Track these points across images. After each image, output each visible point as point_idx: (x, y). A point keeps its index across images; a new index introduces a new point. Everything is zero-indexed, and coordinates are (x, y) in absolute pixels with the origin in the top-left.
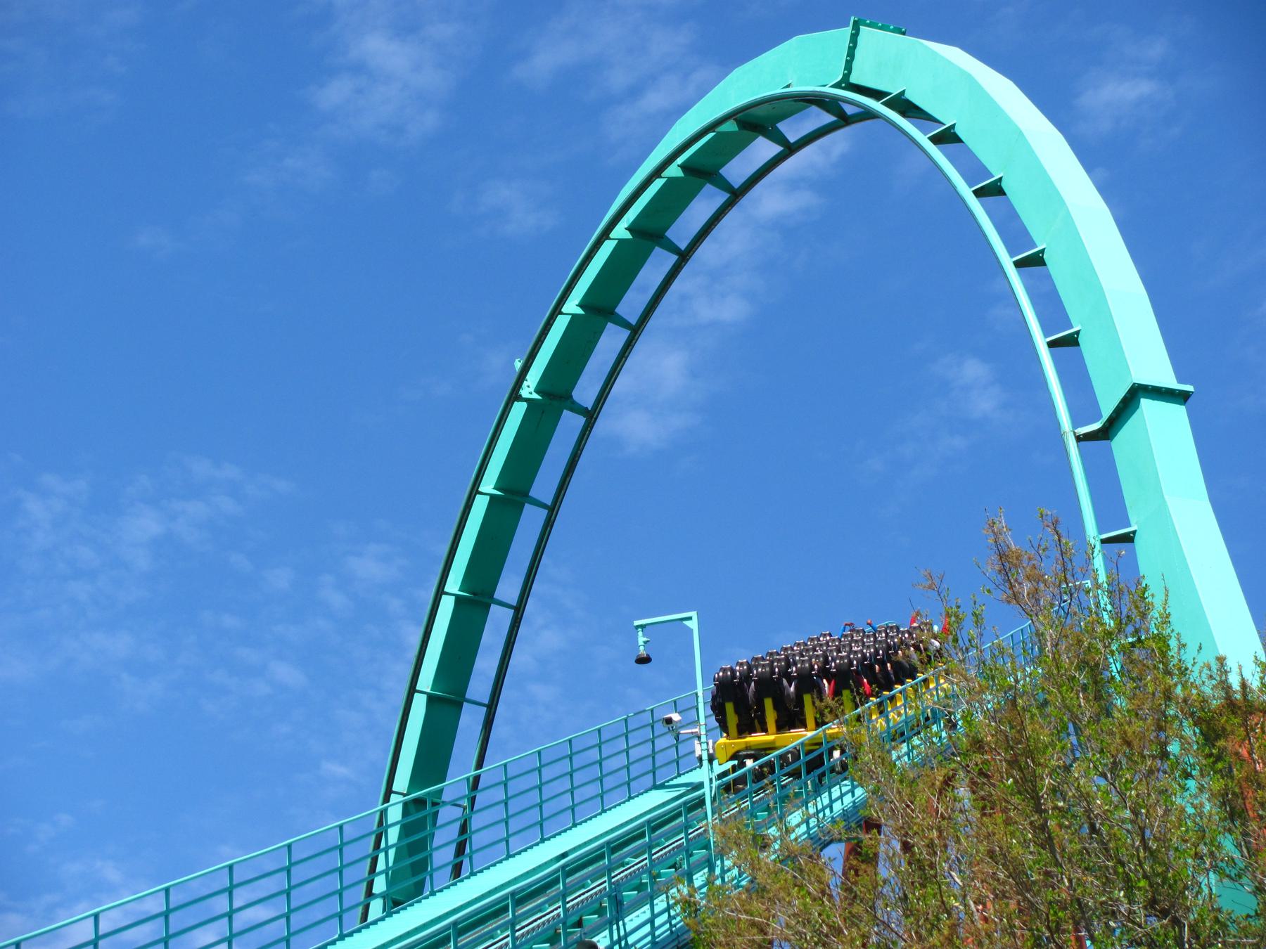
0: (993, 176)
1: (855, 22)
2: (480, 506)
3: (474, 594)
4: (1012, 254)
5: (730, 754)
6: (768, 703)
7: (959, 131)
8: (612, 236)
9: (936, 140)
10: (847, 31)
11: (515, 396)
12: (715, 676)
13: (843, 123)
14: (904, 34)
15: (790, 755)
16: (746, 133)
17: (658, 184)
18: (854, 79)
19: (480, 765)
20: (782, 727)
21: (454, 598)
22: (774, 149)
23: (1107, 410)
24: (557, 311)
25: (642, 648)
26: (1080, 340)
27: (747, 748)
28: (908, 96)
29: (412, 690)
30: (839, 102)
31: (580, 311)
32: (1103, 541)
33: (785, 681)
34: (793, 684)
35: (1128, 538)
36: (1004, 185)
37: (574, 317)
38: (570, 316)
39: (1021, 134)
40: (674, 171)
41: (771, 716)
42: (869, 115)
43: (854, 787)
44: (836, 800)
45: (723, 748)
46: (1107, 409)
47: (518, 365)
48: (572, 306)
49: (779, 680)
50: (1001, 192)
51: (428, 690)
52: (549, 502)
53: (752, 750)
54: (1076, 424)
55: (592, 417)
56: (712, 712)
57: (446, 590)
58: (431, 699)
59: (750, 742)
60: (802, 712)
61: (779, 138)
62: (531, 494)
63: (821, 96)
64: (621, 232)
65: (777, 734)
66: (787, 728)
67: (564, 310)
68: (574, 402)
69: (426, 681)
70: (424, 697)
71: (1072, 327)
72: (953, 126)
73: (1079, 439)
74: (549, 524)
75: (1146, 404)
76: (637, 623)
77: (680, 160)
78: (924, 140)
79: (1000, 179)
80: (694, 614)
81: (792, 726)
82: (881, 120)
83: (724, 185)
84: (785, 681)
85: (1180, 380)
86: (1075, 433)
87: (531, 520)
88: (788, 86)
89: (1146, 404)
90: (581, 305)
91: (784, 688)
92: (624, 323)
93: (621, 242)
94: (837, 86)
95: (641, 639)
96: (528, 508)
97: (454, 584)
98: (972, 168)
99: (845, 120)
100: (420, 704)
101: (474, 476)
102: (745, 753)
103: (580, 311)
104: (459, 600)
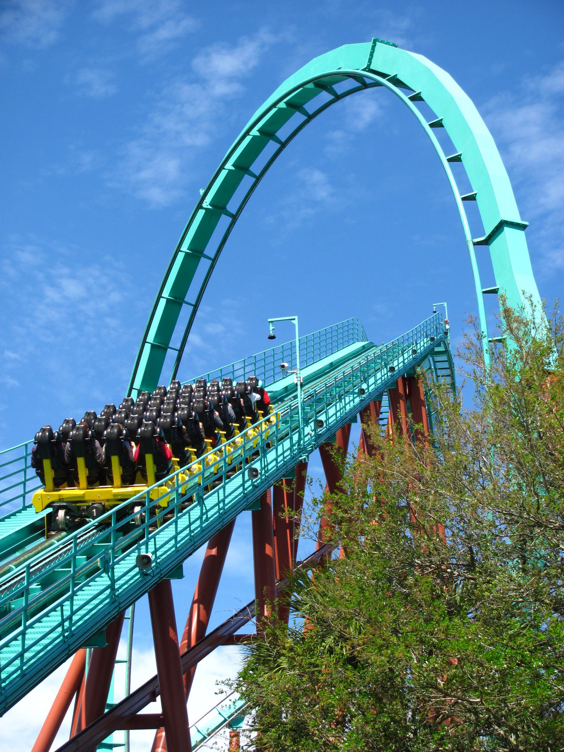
0: (438, 118)
1: (374, 40)
2: (180, 257)
3: (176, 298)
5: (47, 502)
6: (81, 462)
7: (423, 95)
8: (250, 134)
9: (412, 99)
10: (370, 44)
11: (200, 207)
12: (36, 435)
13: (364, 87)
14: (396, 47)
15: (94, 510)
16: (318, 89)
17: (274, 110)
18: (372, 67)
20: (91, 483)
21: (166, 299)
22: (331, 97)
23: (488, 232)
24: (222, 168)
25: (271, 332)
26: (477, 198)
27: (60, 500)
28: (398, 77)
29: (145, 342)
30: (364, 78)
31: (233, 168)
32: (484, 292)
33: (97, 443)
34: (104, 446)
35: (495, 291)
37: (230, 171)
38: (228, 171)
39: (453, 99)
40: (282, 105)
41: (83, 473)
42: (378, 84)
43: (354, 398)
44: (351, 401)
45: (39, 499)
46: (488, 230)
47: (202, 192)
48: (229, 166)
49: (92, 442)
51: (152, 342)
52: (213, 257)
53: (65, 502)
54: (473, 237)
55: (235, 218)
57: (162, 296)
58: (153, 346)
59: (62, 495)
60: (110, 471)
61: (333, 92)
62: (204, 253)
63: (354, 74)
64: (255, 132)
65: (88, 489)
66: (98, 482)
67: (225, 167)
68: (227, 211)
70: (150, 345)
71: (473, 192)
72: (420, 93)
73: (475, 244)
74: (212, 267)
75: (507, 229)
76: (269, 320)
77: (285, 100)
78: (406, 99)
79: (442, 120)
81: (103, 483)
82: (384, 87)
83: (305, 113)
84: (97, 443)
86: (473, 241)
87: (204, 265)
88: (340, 68)
89: (507, 229)
90: (233, 165)
91: (96, 449)
92: (253, 175)
93: (255, 137)
94: (364, 70)
95: (271, 328)
96: (203, 259)
97: (166, 293)
98: (428, 112)
99: (365, 86)
100: (147, 348)
101: (178, 243)
102: (58, 504)
103: (233, 168)
104: (168, 301)
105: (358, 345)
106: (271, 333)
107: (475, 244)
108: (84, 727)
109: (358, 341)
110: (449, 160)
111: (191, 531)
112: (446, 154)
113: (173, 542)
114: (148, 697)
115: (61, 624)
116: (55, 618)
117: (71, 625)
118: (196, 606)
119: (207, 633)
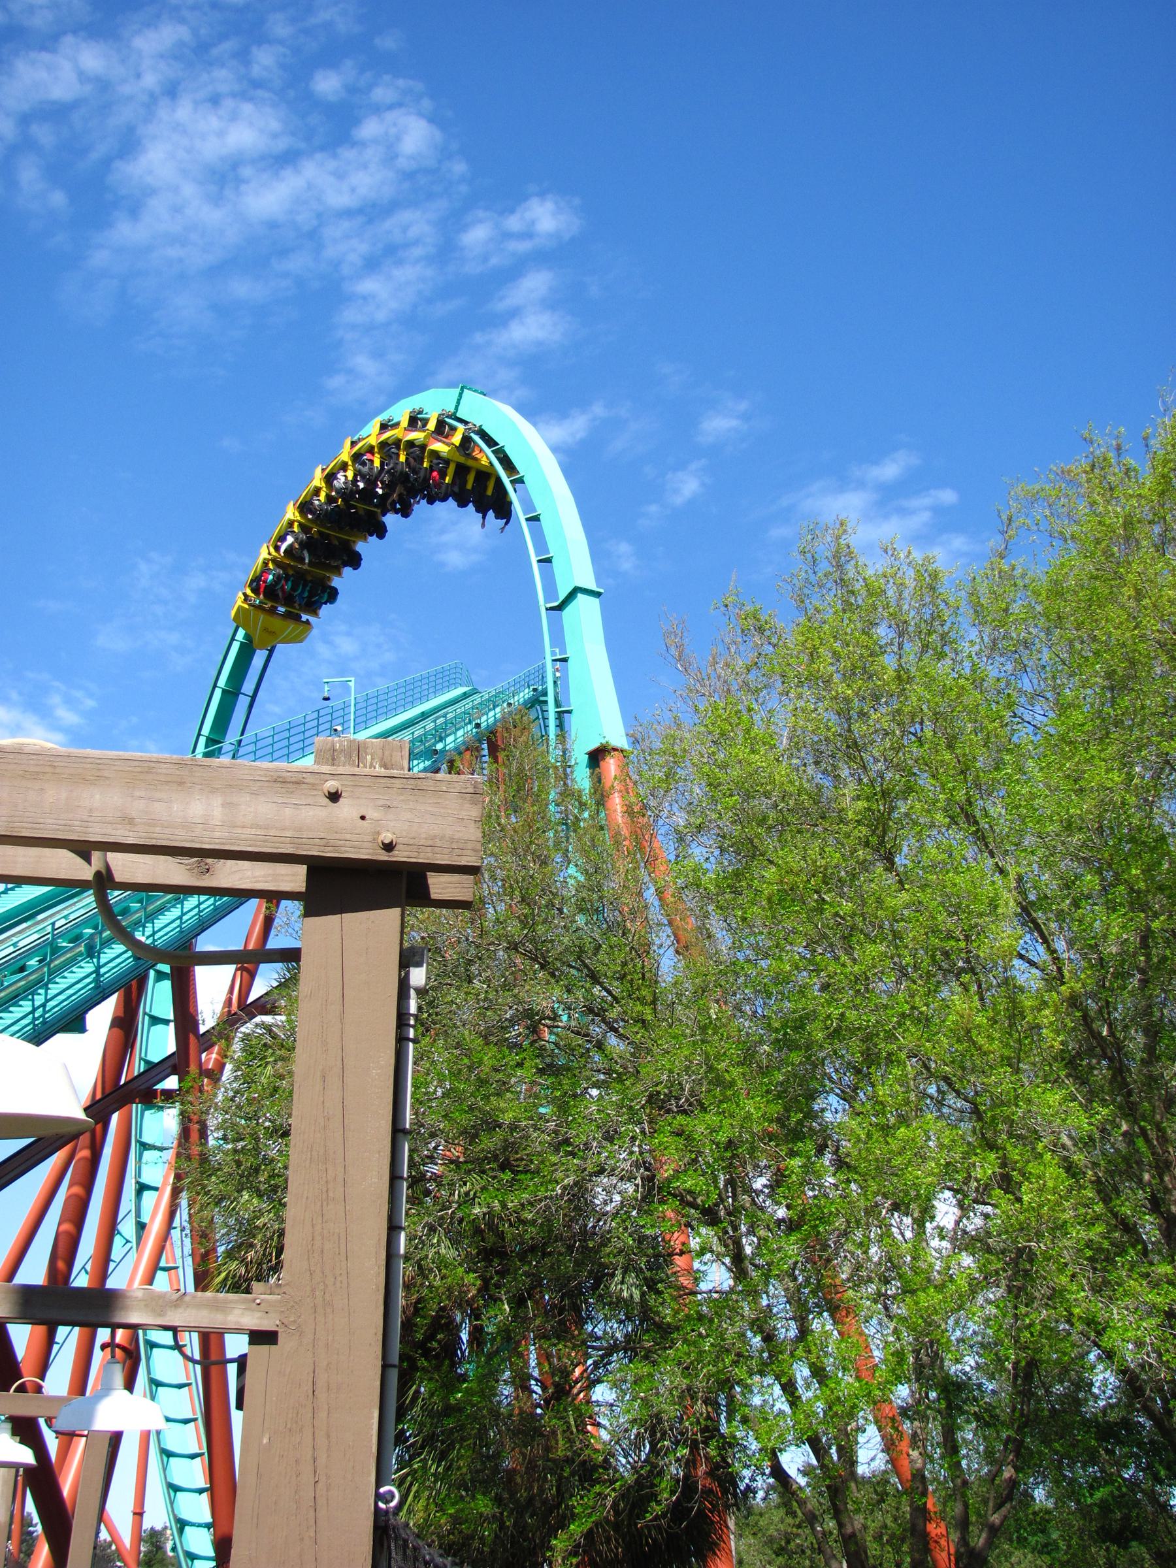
4: (525, 514)
10: (458, 391)
19: (242, 734)
23: (561, 598)
29: (215, 686)
35: (565, 660)
36: (541, 517)
46: (562, 595)
50: (523, 482)
54: (546, 601)
56: (212, 1554)
58: (224, 691)
69: (222, 682)
73: (547, 609)
75: (580, 596)
80: (353, 679)
85: (598, 585)
89: (579, 595)
95: (326, 688)
98: (541, 543)
105: (460, 690)
106: (326, 695)
107: (547, 609)
108: (99, 1096)
109: (461, 685)
110: (528, 520)
111: (200, 911)
112: (525, 513)
113: (178, 922)
114: (169, 1070)
115: (33, 1011)
116: (26, 1006)
117: (45, 1012)
118: (239, 973)
119: (249, 1001)
